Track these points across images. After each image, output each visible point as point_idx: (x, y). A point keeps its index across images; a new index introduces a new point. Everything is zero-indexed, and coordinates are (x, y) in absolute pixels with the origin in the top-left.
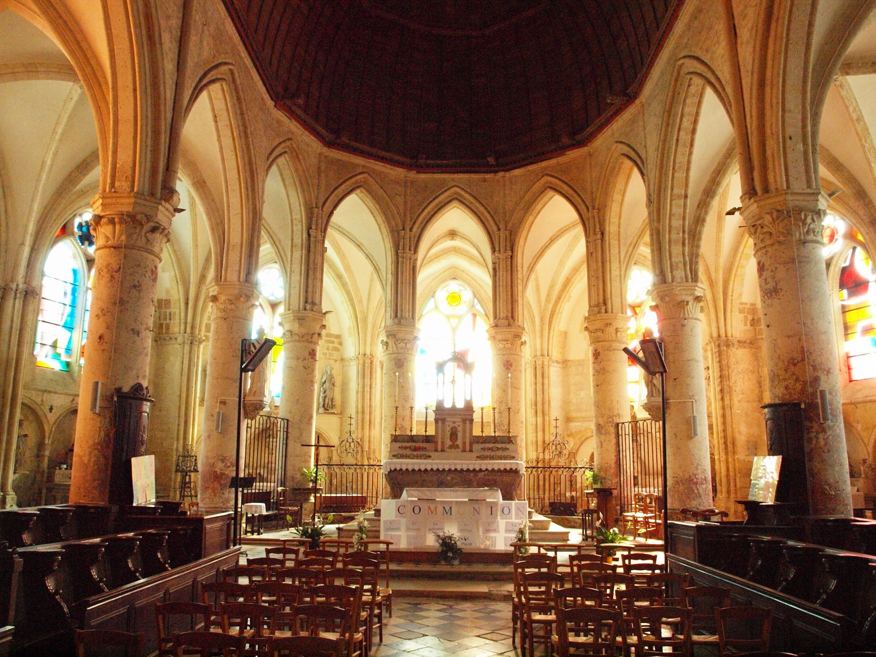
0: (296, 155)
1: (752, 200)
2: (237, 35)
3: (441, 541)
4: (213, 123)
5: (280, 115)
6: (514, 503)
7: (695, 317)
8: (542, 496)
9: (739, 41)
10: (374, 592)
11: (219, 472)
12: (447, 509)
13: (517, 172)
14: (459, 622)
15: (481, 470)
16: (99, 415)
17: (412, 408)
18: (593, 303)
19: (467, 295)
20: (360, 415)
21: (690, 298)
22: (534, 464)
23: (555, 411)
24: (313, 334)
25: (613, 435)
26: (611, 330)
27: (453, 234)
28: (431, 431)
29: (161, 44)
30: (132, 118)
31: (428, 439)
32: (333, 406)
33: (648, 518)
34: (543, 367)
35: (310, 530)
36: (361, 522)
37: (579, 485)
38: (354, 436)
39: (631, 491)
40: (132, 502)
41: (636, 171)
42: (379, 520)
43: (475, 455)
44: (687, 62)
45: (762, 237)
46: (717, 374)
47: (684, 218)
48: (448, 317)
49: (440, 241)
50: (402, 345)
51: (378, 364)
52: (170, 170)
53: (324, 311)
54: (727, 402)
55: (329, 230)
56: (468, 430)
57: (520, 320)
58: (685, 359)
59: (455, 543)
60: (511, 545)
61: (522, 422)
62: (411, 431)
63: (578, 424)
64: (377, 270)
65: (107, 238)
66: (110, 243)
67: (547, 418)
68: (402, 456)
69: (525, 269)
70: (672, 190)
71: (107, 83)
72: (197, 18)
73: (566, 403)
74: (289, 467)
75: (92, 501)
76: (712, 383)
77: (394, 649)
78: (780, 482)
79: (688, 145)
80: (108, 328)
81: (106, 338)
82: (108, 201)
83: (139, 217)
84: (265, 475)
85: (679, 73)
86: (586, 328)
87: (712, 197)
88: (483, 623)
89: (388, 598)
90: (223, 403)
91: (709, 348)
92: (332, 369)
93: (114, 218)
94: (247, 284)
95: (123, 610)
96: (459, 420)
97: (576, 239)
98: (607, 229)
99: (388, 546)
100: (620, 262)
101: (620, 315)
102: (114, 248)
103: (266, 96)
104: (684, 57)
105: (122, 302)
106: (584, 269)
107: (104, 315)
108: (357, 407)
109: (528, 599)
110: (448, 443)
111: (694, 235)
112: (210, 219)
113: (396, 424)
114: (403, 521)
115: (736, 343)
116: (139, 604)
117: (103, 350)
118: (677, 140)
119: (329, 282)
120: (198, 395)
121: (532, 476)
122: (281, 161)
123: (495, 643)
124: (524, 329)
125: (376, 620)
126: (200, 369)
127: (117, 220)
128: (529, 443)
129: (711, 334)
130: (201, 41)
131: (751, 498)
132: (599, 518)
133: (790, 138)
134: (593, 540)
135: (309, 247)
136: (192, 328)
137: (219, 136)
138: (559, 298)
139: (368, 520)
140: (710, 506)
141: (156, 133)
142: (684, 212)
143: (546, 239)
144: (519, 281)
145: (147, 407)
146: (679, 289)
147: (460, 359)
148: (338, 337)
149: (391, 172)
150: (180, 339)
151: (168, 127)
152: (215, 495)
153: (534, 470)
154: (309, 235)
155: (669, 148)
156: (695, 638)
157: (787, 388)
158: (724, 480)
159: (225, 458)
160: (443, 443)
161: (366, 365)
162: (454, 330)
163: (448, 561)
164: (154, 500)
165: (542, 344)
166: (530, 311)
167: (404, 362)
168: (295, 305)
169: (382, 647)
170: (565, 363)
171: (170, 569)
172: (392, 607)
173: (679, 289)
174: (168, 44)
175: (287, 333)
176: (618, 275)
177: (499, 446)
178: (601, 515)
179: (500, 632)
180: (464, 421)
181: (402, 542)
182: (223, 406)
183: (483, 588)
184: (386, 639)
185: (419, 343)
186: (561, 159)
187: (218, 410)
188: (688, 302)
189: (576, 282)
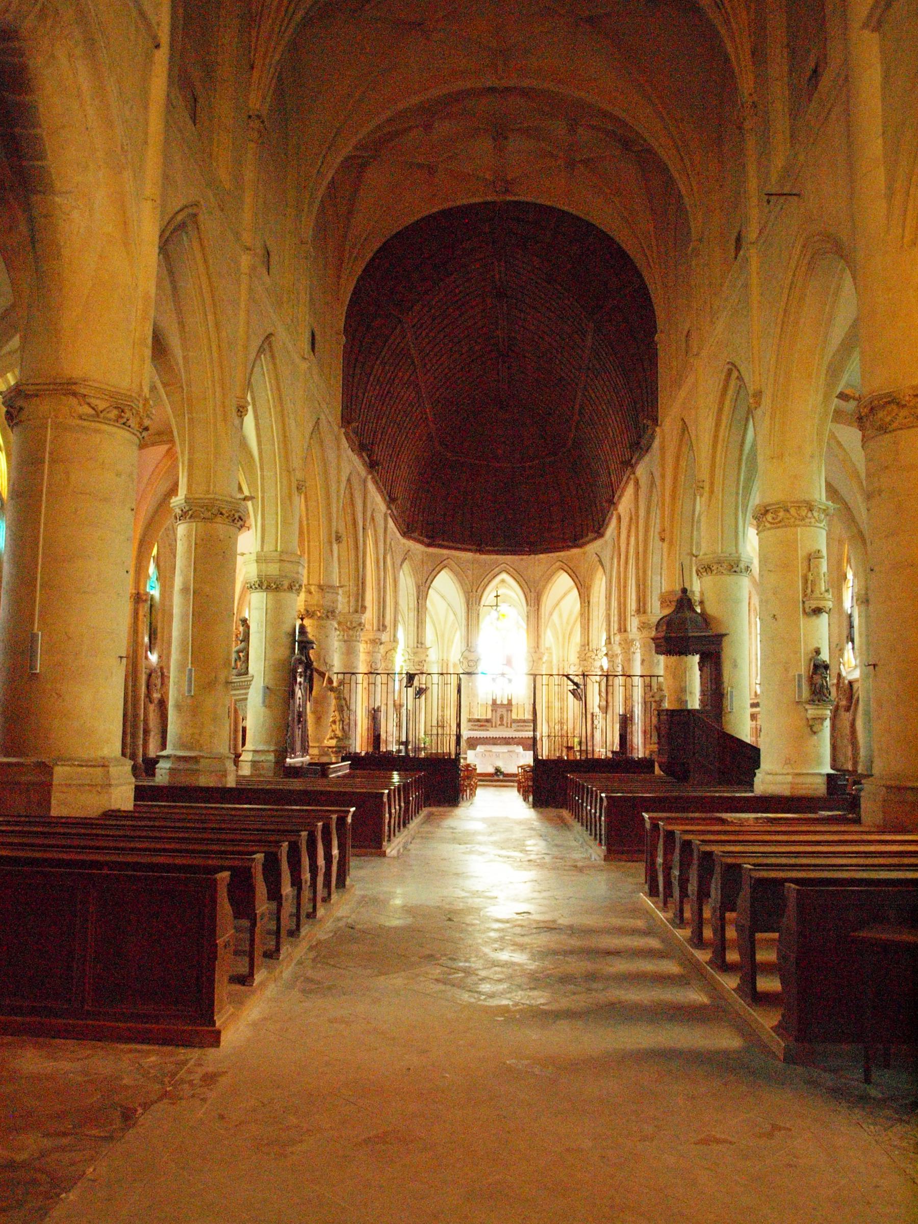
28: (489, 717)
31: (487, 721)
68: (473, 730)
69: (547, 614)
110: (499, 723)
144: (543, 624)
163: (498, 775)
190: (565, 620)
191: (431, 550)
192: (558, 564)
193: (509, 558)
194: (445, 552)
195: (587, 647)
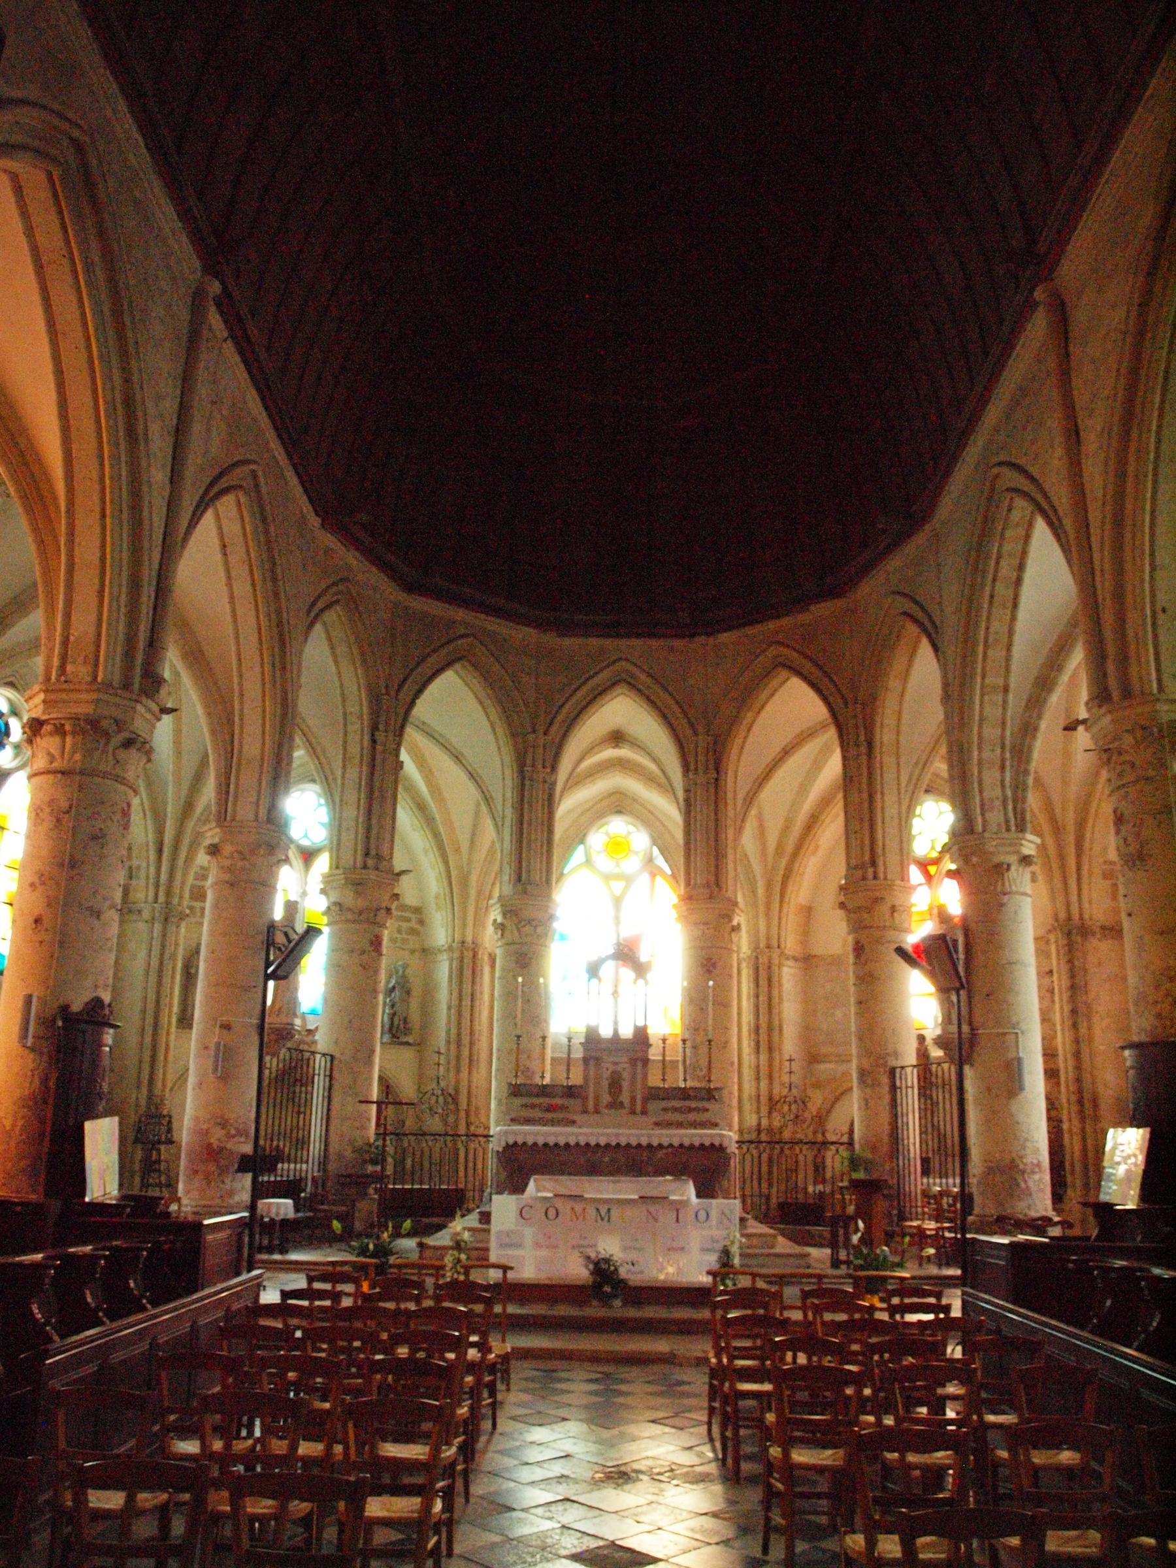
0: (354, 605)
1: (1103, 710)
2: (264, 414)
3: (591, 1267)
4: (219, 557)
5: (329, 540)
6: (716, 1204)
7: (1022, 890)
8: (765, 1191)
9: (1083, 449)
10: (483, 1347)
11: (215, 1145)
12: (603, 1212)
13: (724, 637)
14: (621, 1400)
15: (660, 1146)
16: (32, 1049)
17: (544, 1038)
18: (853, 862)
19: (640, 839)
20: (453, 1047)
21: (1013, 859)
22: (754, 1136)
23: (790, 1045)
24: (378, 910)
25: (887, 1088)
26: (885, 908)
27: (617, 737)
28: (576, 1078)
29: (147, 440)
30: (97, 562)
31: (571, 1092)
32: (407, 1031)
33: (943, 1229)
34: (769, 967)
35: (371, 1247)
36: (458, 1234)
37: (829, 1175)
38: (443, 1084)
39: (917, 1183)
40: (84, 1195)
41: (925, 641)
42: (488, 1231)
43: (650, 1119)
44: (1005, 470)
45: (1119, 769)
46: (1066, 983)
47: (1004, 724)
48: (608, 877)
49: (596, 750)
50: (528, 929)
51: (486, 958)
52: (154, 645)
53: (397, 869)
54: (1083, 1030)
55: (410, 731)
56: (639, 1077)
57: (730, 888)
58: (1004, 962)
59: (616, 1269)
60: (709, 1273)
61: (732, 1063)
62: (543, 1077)
63: (832, 1066)
64: (488, 799)
65: (52, 758)
66: (56, 765)
67: (776, 1054)
68: (528, 1121)
70: (983, 677)
71: (58, 508)
72: (203, 392)
73: (808, 1032)
74: (333, 1138)
75: (17, 1192)
76: (1057, 998)
77: (514, 1439)
78: (1145, 1172)
79: (1010, 605)
80: (49, 905)
81: (46, 922)
82: (53, 696)
83: (105, 724)
84: (287, 1149)
85: (992, 489)
86: (842, 905)
87: (1050, 691)
88: (661, 1401)
89: (505, 1358)
90: (227, 1027)
91: (1052, 937)
92: (405, 966)
93: (63, 725)
94: (269, 826)
95: (92, 1368)
96: (625, 1059)
97: (825, 753)
98: (878, 737)
99: (505, 1272)
100: (899, 789)
101: (898, 882)
102: (63, 773)
103: (307, 509)
104: (1000, 464)
105: (73, 864)
106: (838, 808)
107: (43, 883)
108: (448, 1032)
109: (731, 1358)
110: (606, 1099)
111: (1021, 753)
112: (209, 714)
113: (517, 1065)
114: (529, 1233)
115: (1098, 930)
116: (117, 1357)
117: (41, 942)
118: (992, 597)
119: (405, 818)
120: (175, 1009)
121: (748, 1157)
122: (330, 616)
123: (679, 1432)
124: (736, 904)
125: (485, 1394)
126: (179, 965)
127: (68, 728)
128: (745, 1096)
129: (1056, 915)
130: (208, 430)
131: (1103, 1198)
132: (857, 1230)
133: (1164, 610)
134: (848, 1268)
135: (373, 759)
136: (169, 893)
137: (229, 578)
138: (799, 847)
139: (470, 1229)
140: (1046, 1210)
141: (135, 585)
142: (1004, 714)
143: (777, 748)
144: (729, 822)
145: (109, 1036)
146: (994, 843)
147: (626, 954)
148: (418, 910)
149: (514, 633)
150: (146, 914)
151: (154, 573)
152: (209, 1183)
153: (787, 1146)
154: (374, 741)
155: (979, 610)
156: (991, 1418)
157: (1159, 1016)
158: (1078, 1166)
159: (227, 1121)
160: (597, 1098)
161: (465, 961)
162: (618, 902)
163: (605, 1300)
164: (115, 1193)
165: (768, 927)
166: (748, 867)
167: (530, 959)
168: (347, 859)
169: (496, 1437)
170: (807, 961)
171: (149, 1306)
172: (512, 1376)
173: (994, 843)
174: (159, 443)
175: (333, 908)
176: (896, 815)
177: (693, 1104)
178: (861, 1224)
179: (687, 1415)
180: (633, 1062)
181: (528, 1270)
182: (225, 1032)
183: (662, 1345)
184: (503, 1424)
185: (555, 925)
186: (805, 618)
187: (216, 1040)
188: (1009, 866)
189: (827, 821)
190: (772, 844)
191: (418, 604)
192: (772, 651)
193: (636, 645)
194: (460, 614)
195: (871, 871)
